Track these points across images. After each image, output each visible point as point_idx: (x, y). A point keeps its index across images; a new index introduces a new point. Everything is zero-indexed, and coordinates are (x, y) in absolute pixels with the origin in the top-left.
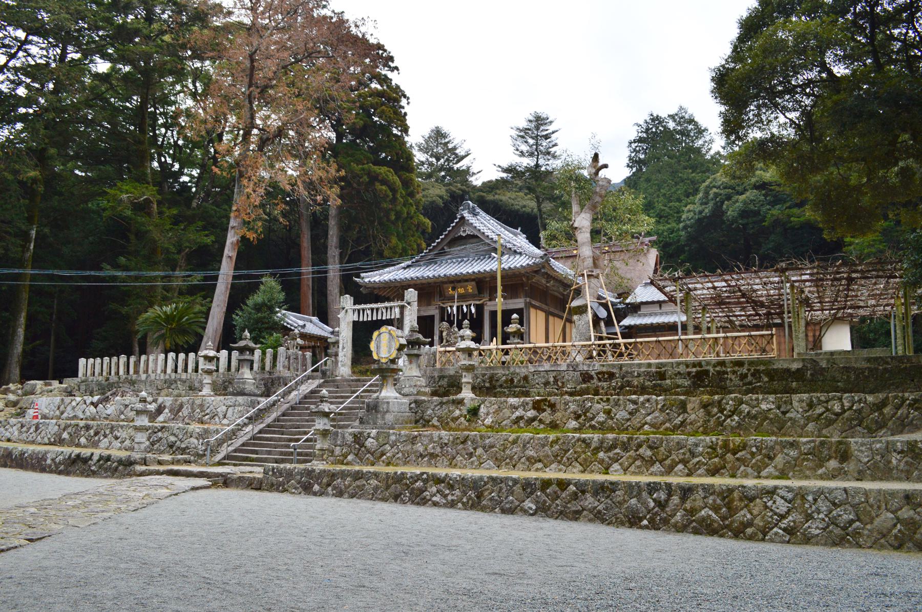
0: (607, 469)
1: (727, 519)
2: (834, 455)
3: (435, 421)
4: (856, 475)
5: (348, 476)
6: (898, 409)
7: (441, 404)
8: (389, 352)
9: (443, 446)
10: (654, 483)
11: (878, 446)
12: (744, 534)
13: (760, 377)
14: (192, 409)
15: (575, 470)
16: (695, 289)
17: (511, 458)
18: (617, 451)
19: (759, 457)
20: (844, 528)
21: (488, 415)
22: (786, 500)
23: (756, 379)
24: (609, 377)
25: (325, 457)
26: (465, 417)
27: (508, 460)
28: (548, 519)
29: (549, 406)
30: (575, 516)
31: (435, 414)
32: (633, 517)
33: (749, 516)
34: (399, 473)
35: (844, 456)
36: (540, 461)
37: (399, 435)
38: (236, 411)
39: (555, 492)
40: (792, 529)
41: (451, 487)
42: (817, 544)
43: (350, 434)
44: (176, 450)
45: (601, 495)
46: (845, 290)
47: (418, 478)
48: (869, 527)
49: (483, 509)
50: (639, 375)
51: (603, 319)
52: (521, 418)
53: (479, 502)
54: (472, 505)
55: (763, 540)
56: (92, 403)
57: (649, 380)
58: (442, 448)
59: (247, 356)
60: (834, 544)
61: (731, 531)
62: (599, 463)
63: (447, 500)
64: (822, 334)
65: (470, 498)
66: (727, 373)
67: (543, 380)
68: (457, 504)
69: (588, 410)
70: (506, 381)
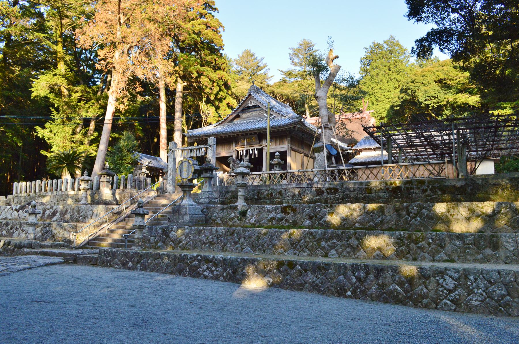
1: (409, 292)
2: (488, 245)
3: (218, 221)
7: (223, 209)
9: (218, 236)
10: (356, 265)
12: (422, 304)
13: (436, 191)
14: (73, 212)
15: (305, 254)
16: (394, 135)
18: (334, 241)
19: (434, 246)
20: (498, 301)
21: (252, 216)
22: (453, 279)
23: (433, 193)
24: (334, 192)
25: (140, 243)
26: (238, 217)
28: (280, 290)
30: (300, 287)
32: (341, 289)
33: (425, 290)
34: (183, 255)
39: (286, 270)
40: (457, 301)
41: (216, 265)
43: (160, 229)
45: (318, 272)
46: (492, 136)
47: (195, 258)
50: (354, 190)
51: (334, 155)
53: (235, 277)
54: (230, 279)
55: (436, 308)
56: (16, 210)
57: (361, 194)
58: (218, 238)
61: (412, 301)
62: (321, 249)
63: (213, 274)
64: (476, 167)
65: (228, 273)
66: (413, 189)
68: (219, 277)
69: (317, 214)
70: (268, 195)
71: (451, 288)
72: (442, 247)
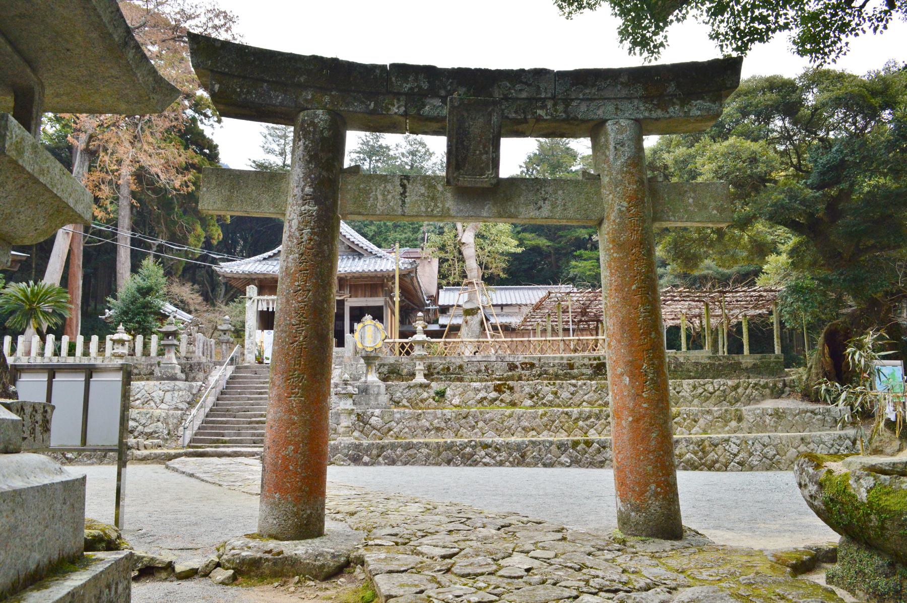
0: (586, 433)
3: (405, 402)
4: (748, 430)
5: (398, 447)
6: (746, 389)
8: (374, 342)
11: (758, 411)
17: (510, 429)
18: (592, 420)
20: (771, 460)
27: (507, 430)
29: (508, 389)
31: (404, 396)
33: (716, 456)
35: (740, 419)
36: (533, 430)
37: (404, 413)
38: (176, 395)
41: (498, 450)
42: (758, 470)
44: (139, 435)
48: (784, 458)
49: (528, 465)
50: (554, 366)
52: (485, 398)
53: (524, 460)
55: (726, 470)
59: (172, 341)
60: (767, 470)
67: (476, 369)
70: (443, 369)
71: (736, 453)
72: (696, 421)
